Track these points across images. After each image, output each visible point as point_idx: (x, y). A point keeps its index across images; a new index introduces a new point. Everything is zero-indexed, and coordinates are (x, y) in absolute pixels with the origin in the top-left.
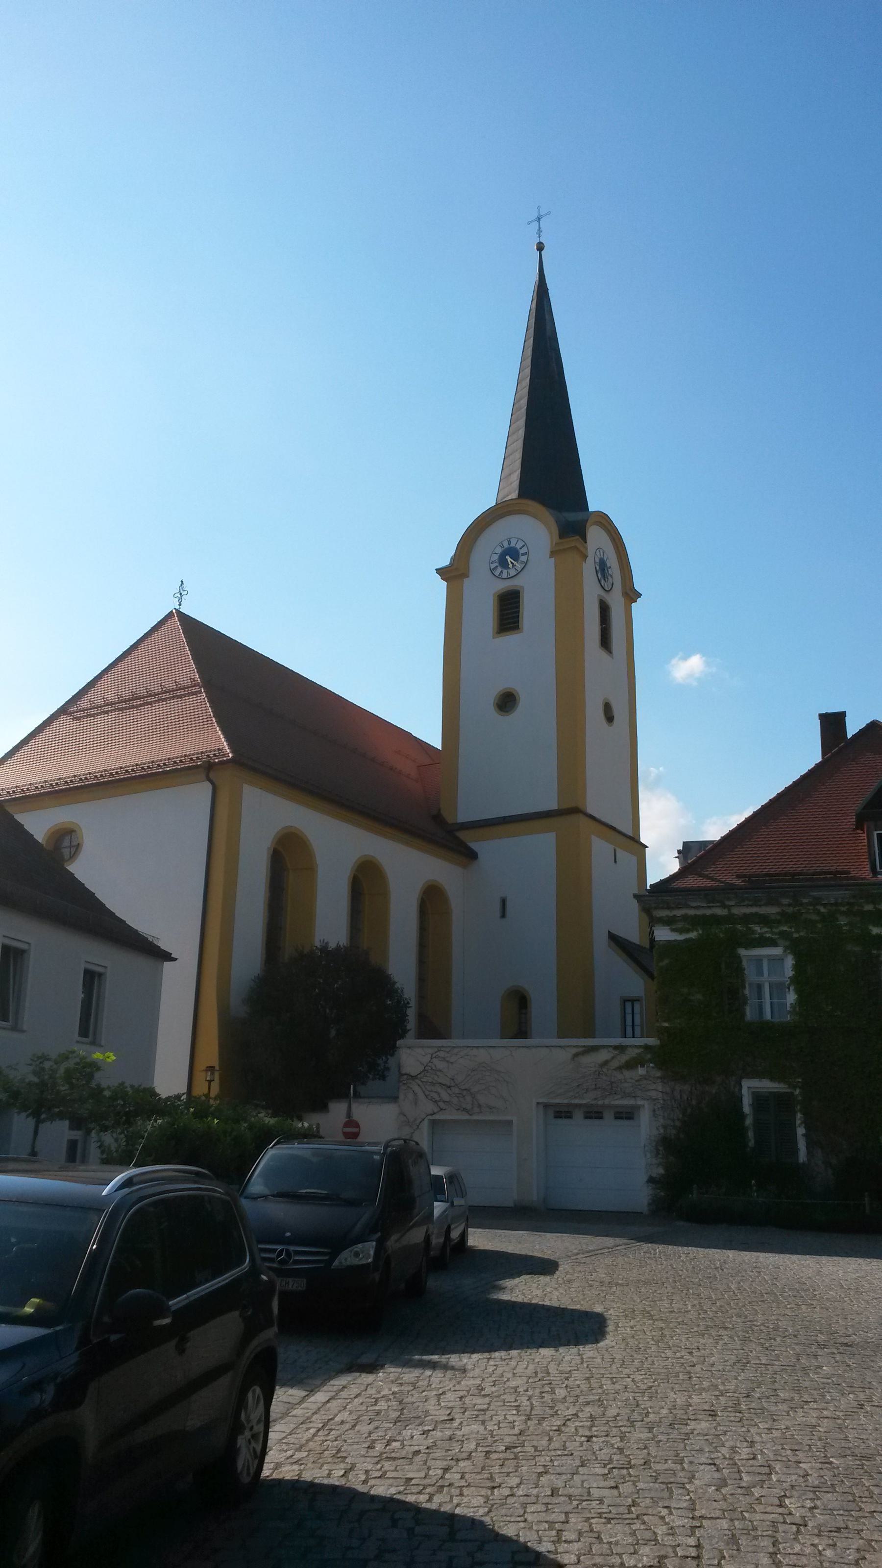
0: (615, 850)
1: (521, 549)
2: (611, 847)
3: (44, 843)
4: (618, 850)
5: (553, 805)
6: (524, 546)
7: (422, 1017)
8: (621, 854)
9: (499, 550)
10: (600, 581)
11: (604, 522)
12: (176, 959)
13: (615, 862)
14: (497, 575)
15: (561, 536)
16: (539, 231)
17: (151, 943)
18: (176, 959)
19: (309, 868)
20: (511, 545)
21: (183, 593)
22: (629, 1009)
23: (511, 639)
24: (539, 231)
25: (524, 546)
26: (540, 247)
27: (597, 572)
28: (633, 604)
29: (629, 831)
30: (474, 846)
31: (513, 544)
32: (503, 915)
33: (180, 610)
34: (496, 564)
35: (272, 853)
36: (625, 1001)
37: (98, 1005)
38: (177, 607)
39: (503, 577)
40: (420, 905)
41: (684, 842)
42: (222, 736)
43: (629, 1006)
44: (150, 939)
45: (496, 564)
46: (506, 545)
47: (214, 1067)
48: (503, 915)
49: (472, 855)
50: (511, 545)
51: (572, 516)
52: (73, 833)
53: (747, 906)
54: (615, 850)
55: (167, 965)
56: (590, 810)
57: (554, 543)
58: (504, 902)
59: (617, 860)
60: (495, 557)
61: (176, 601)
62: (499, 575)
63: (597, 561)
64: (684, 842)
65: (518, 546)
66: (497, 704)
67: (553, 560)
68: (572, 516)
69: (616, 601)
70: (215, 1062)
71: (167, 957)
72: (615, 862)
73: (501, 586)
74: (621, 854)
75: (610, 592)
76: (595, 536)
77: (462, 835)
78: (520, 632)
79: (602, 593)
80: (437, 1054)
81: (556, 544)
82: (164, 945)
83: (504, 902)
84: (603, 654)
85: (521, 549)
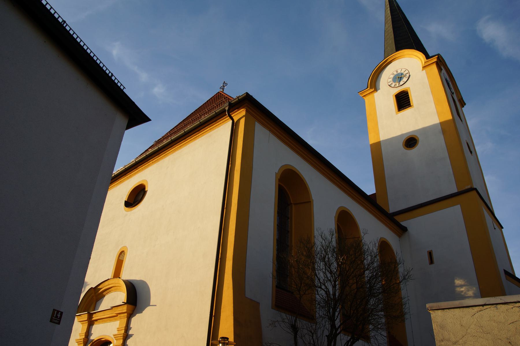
1: (404, 72)
5: (455, 190)
23: (407, 112)
30: (403, 224)
32: (431, 262)
48: (431, 262)
49: (404, 230)
50: (398, 72)
58: (430, 254)
65: (402, 72)
67: (424, 71)
81: (425, 62)
83: (430, 254)
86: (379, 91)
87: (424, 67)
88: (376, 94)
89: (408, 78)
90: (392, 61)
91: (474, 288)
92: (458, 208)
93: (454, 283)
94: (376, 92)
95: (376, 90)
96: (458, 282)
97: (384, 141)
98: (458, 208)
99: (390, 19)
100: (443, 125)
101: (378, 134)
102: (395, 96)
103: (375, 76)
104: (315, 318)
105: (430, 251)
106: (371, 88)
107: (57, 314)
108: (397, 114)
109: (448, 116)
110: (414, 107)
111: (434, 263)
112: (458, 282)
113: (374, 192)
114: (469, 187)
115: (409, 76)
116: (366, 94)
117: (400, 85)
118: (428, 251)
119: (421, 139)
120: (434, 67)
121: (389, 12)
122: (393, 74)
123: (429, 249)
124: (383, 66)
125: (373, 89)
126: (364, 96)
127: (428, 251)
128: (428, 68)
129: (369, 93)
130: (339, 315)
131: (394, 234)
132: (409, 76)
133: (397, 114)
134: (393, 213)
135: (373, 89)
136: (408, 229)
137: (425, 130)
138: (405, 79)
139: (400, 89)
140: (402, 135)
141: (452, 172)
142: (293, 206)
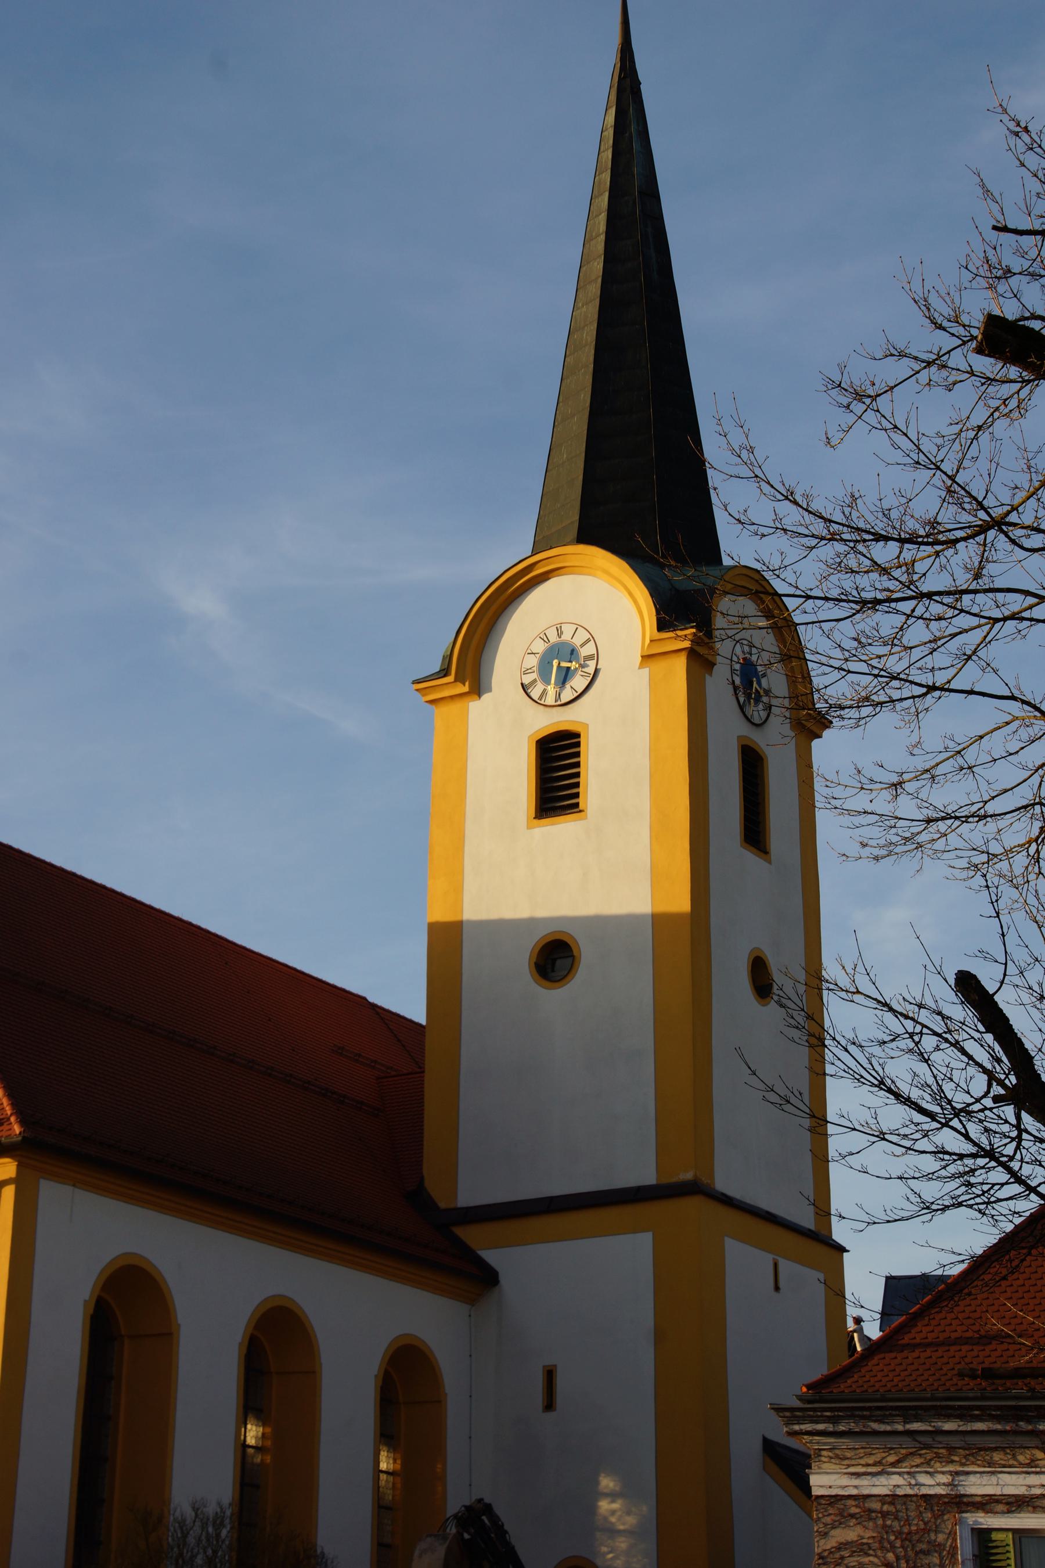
0: (776, 1265)
1: (582, 645)
2: (768, 1259)
4: (783, 1263)
5: (647, 1175)
6: (588, 641)
8: (786, 1267)
9: (540, 647)
13: (777, 1288)
14: (536, 699)
20: (563, 637)
25: (588, 641)
27: (735, 688)
28: (816, 744)
29: (806, 1219)
30: (491, 1256)
31: (566, 636)
32: (549, 1405)
35: (91, 1311)
39: (546, 703)
40: (382, 1388)
41: (890, 1281)
48: (549, 1405)
49: (488, 1278)
51: (684, 577)
53: (979, 1466)
54: (776, 1265)
57: (647, 641)
58: (550, 1374)
59: (781, 1285)
60: (533, 662)
62: (540, 698)
64: (890, 1281)
65: (577, 641)
66: (536, 964)
68: (684, 577)
72: (777, 1288)
73: (546, 722)
74: (786, 1267)
77: (469, 1234)
78: (581, 819)
81: (651, 641)
83: (550, 1374)
84: (750, 858)
85: (582, 645)
86: (486, 697)
87: (647, 658)
88: (476, 707)
89: (589, 679)
90: (551, 575)
91: (645, 1508)
93: (597, 1483)
94: (476, 697)
96: (607, 1483)
97: (469, 922)
98: (646, 1239)
99: (597, 278)
100: (659, 921)
101: (457, 889)
102: (537, 742)
103: (482, 625)
105: (543, 1371)
106: (460, 679)
107: (404, 1475)
108: (529, 828)
109: (681, 902)
110: (586, 818)
111: (555, 1410)
112: (607, 1483)
113: (726, 561)
114: (689, 1176)
115: (596, 671)
117: (559, 703)
118: (544, 1367)
119: (587, 953)
120: (680, 664)
124: (518, 588)
125: (467, 684)
126: (432, 702)
127: (544, 1367)
128: (661, 665)
129: (452, 697)
132: (596, 671)
135: (467, 684)
136: (503, 1279)
138: (578, 682)
139: (556, 720)
140: (531, 923)
141: (654, 1111)
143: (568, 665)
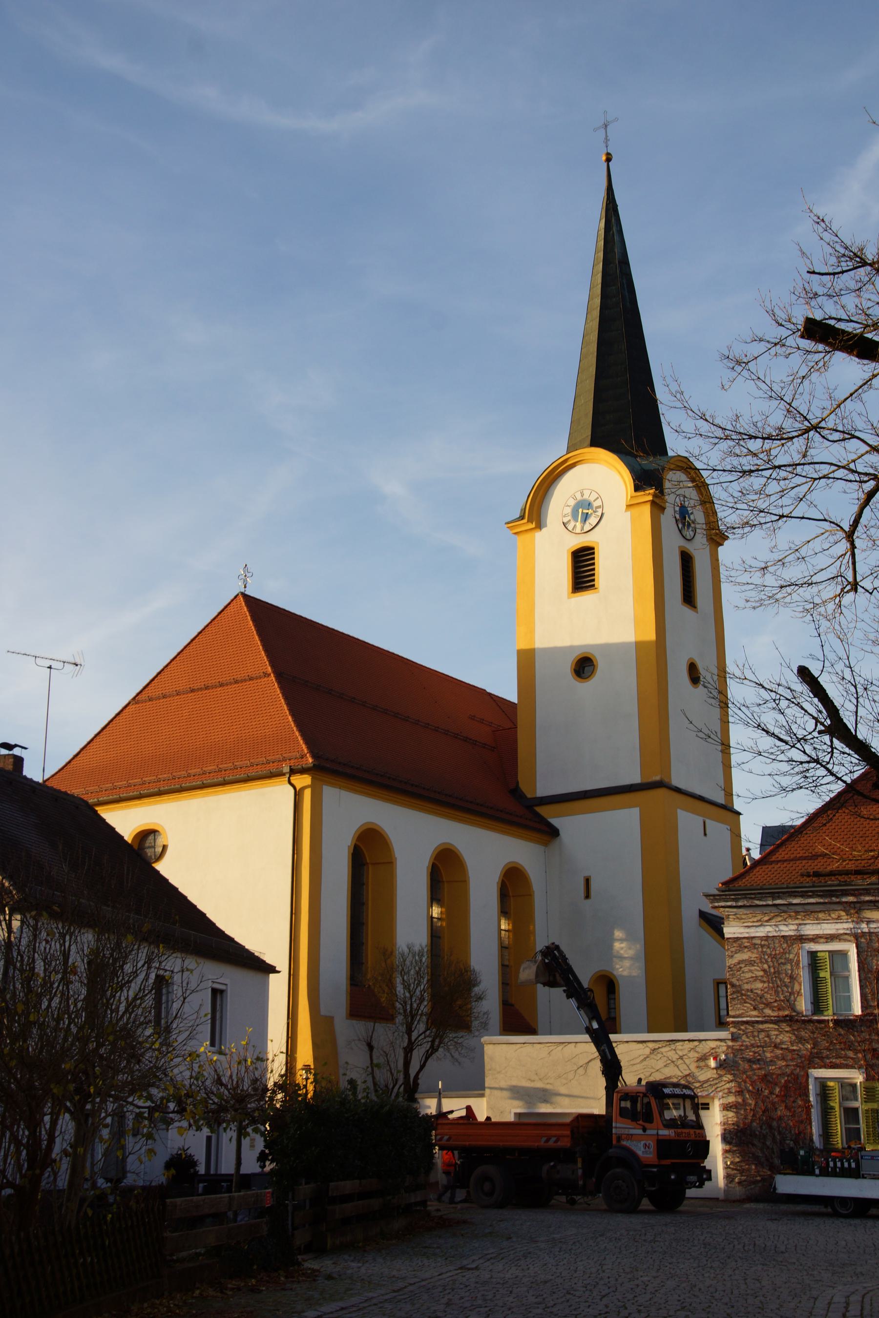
0: (704, 823)
2: (700, 820)
3: (130, 842)
4: (708, 822)
5: (636, 779)
6: (598, 498)
7: (507, 1005)
9: (572, 503)
10: (680, 531)
11: (685, 466)
12: (279, 972)
13: (705, 834)
14: (571, 529)
15: (637, 488)
16: (607, 140)
17: (258, 958)
18: (279, 972)
19: (389, 863)
20: (584, 497)
21: (248, 575)
22: (722, 992)
23: (586, 598)
24: (607, 140)
25: (598, 498)
26: (609, 160)
27: (677, 521)
28: (720, 549)
30: (555, 822)
31: (586, 497)
32: (587, 896)
33: (246, 593)
34: (569, 518)
35: (352, 851)
36: (718, 983)
37: (221, 1017)
38: (243, 590)
42: (299, 738)
43: (722, 989)
44: (256, 954)
45: (569, 518)
46: (579, 497)
47: (309, 1066)
49: (553, 833)
50: (584, 497)
52: (157, 833)
54: (704, 823)
55: (272, 976)
56: (675, 782)
59: (707, 832)
60: (568, 510)
61: (241, 583)
62: (573, 529)
63: (677, 509)
65: (592, 499)
67: (629, 513)
68: (648, 463)
69: (699, 549)
70: (310, 1061)
71: (272, 969)
72: (705, 834)
73: (577, 542)
75: (694, 540)
76: (673, 478)
77: (542, 810)
79: (682, 542)
80: (768, 444)
82: (269, 960)
83: (587, 881)
84: (686, 610)
86: (544, 530)
87: (629, 506)
88: (539, 535)
91: (638, 946)
92: (636, 811)
93: (613, 934)
95: (540, 526)
96: (618, 934)
98: (636, 811)
101: (531, 631)
104: (116, 1119)
106: (530, 521)
108: (569, 598)
109: (650, 635)
113: (670, 453)
115: (602, 514)
116: (521, 532)
119: (601, 664)
121: (600, 276)
122: (575, 498)
123: (587, 874)
128: (636, 510)
129: (526, 531)
130: (120, 1013)
131: (537, 845)
132: (602, 514)
133: (569, 598)
134: (542, 798)
136: (561, 832)
137: (608, 648)
140: (571, 648)
142: (370, 866)
143: (587, 511)
